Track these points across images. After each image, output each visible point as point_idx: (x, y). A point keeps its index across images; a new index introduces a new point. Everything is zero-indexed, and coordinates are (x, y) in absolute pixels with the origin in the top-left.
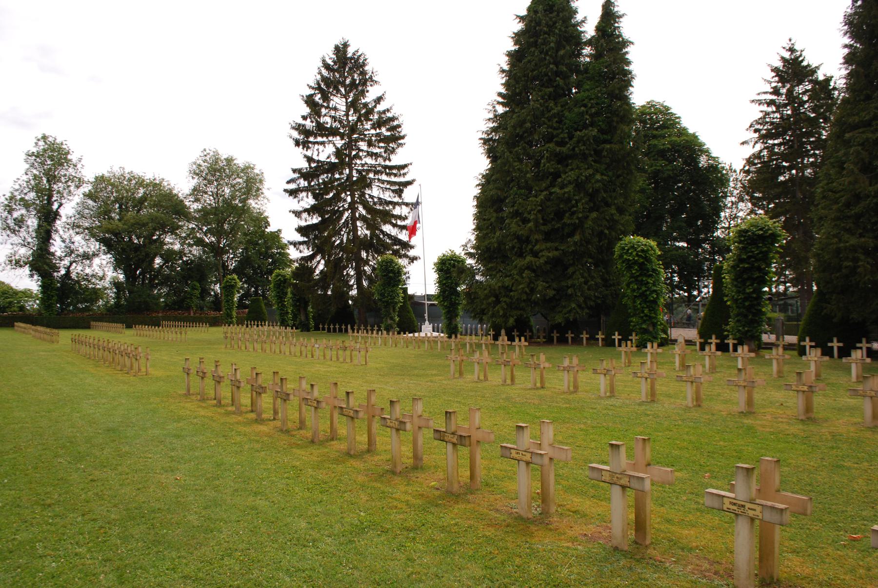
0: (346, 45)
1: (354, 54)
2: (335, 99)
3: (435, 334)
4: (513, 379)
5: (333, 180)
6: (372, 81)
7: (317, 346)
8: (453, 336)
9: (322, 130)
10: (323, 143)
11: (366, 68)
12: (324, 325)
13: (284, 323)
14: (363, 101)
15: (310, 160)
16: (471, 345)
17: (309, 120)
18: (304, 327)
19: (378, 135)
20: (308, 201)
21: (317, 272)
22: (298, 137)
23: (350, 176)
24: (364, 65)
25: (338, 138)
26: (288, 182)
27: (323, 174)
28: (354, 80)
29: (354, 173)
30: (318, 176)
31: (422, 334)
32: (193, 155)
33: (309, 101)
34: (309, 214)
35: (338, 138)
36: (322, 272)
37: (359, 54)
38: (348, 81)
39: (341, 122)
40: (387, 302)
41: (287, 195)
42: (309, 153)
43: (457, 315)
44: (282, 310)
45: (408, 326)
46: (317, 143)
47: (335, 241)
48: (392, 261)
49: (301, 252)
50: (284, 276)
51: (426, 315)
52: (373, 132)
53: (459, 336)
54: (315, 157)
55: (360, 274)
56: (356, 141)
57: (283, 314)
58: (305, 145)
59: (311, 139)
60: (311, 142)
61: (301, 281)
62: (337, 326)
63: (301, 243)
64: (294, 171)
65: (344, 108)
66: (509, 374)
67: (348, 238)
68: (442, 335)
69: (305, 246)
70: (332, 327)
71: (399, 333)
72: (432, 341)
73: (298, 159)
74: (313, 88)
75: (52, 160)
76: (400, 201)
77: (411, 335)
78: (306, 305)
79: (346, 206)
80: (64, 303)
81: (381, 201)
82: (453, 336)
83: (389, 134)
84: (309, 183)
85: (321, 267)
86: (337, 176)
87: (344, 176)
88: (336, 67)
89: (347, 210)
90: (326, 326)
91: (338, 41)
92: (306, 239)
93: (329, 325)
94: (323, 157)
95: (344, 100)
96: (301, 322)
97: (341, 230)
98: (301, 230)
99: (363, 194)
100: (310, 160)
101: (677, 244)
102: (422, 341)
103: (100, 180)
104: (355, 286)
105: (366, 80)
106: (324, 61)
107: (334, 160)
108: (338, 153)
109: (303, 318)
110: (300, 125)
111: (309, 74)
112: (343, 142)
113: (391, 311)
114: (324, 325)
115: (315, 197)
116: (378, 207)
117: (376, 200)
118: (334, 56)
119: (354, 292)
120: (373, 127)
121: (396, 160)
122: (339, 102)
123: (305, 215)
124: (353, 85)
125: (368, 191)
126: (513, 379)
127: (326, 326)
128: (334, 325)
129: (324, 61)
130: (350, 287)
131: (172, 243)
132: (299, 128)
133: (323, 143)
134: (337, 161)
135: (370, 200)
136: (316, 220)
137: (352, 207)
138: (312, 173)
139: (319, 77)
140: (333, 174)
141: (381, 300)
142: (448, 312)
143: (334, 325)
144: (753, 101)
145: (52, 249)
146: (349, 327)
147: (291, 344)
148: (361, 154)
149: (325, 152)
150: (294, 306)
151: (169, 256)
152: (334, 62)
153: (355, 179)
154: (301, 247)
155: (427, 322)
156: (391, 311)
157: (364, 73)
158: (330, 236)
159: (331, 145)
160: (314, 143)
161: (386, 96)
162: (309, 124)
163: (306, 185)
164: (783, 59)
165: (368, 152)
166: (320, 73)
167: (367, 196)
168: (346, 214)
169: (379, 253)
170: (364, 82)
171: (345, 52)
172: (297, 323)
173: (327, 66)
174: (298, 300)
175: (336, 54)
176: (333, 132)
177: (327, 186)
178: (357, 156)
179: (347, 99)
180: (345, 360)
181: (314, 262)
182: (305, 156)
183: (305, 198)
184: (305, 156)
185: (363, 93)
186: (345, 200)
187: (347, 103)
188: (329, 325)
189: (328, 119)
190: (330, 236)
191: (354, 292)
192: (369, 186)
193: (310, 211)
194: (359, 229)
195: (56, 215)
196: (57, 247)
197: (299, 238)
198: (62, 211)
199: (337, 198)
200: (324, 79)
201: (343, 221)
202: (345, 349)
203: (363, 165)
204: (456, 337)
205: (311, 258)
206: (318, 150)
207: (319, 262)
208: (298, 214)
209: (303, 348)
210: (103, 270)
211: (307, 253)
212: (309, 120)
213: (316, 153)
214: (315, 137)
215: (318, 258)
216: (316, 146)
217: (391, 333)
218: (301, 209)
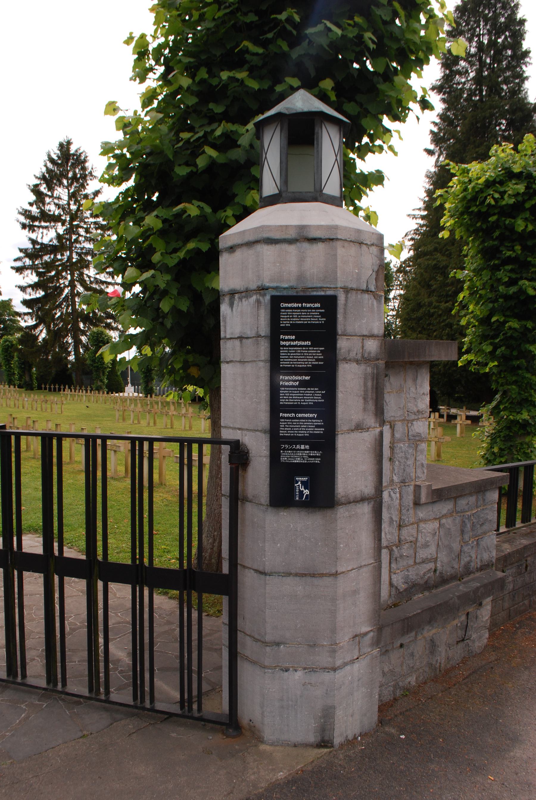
0: (69, 143)
1: (76, 151)
2: (58, 189)
3: (136, 394)
4: (155, 423)
5: (55, 260)
6: (92, 175)
7: (26, 399)
8: (149, 396)
9: (45, 216)
10: (46, 227)
11: (87, 165)
12: (45, 385)
13: (10, 382)
14: (84, 193)
15: (34, 242)
16: (162, 403)
17: (35, 206)
18: (28, 386)
19: (95, 223)
20: (33, 278)
21: (40, 339)
22: (24, 221)
23: (70, 258)
24: (85, 161)
25: (60, 224)
26: (15, 260)
27: (46, 254)
28: (75, 174)
29: (75, 256)
30: (41, 257)
31: (126, 394)
33: (35, 190)
34: (33, 289)
35: (60, 224)
36: (44, 339)
37: (81, 151)
38: (70, 175)
39: (64, 209)
40: (97, 367)
41: (14, 271)
42: (33, 236)
43: (153, 380)
44: (8, 371)
45: (115, 386)
46: (43, 227)
47: (56, 314)
48: (102, 333)
49: (25, 321)
50: (11, 342)
51: (129, 379)
52: (92, 220)
53: (153, 396)
54: (39, 240)
55: (77, 342)
56: (78, 226)
57: (10, 374)
58: (32, 228)
59: (37, 223)
60: (36, 226)
61: (25, 346)
62: (57, 386)
63: (25, 314)
64: (21, 250)
65: (66, 198)
66: (169, 421)
67: (67, 311)
68: (141, 395)
69: (29, 317)
70: (52, 387)
71: (108, 393)
72: (133, 400)
73: (23, 239)
74: (39, 178)
76: (113, 282)
77: (117, 394)
78: (30, 368)
79: (67, 283)
81: (98, 281)
82: (149, 396)
84: (33, 262)
85: (43, 335)
86: (59, 257)
87: (65, 258)
88: (60, 162)
89: (68, 287)
90: (48, 386)
91: (62, 139)
92: (31, 311)
93: (50, 385)
94: (46, 241)
95: (66, 190)
96: (25, 382)
97: (62, 304)
98: (26, 303)
99: (82, 274)
100: (34, 242)
102: (124, 400)
104: (73, 353)
105: (86, 176)
106: (49, 156)
107: (55, 242)
108: (59, 237)
109: (27, 379)
110: (26, 211)
111: (38, 167)
112: (65, 228)
113: (101, 375)
114: (45, 385)
115: (39, 274)
116: (94, 286)
117: (92, 279)
118: (58, 152)
119: (72, 358)
120: (92, 216)
122: (62, 193)
123: (29, 290)
124: (75, 178)
125: (86, 272)
126: (155, 423)
127: (48, 386)
128: (55, 385)
129: (49, 156)
130: (69, 354)
132: (26, 214)
133: (46, 227)
134: (57, 244)
135: (87, 279)
136: (40, 293)
137: (72, 284)
138: (36, 252)
139: (44, 170)
140: (55, 255)
141: (92, 365)
142: (146, 377)
143: (55, 385)
144: (409, 215)
146: (67, 387)
147: (7, 398)
148: (80, 238)
149: (48, 236)
150: (20, 368)
152: (58, 156)
153: (74, 260)
154: (26, 317)
155: (130, 385)
156: (101, 375)
157: (84, 169)
158: (51, 310)
159: (54, 230)
160: (39, 227)
161: (103, 190)
162: (34, 210)
163: (31, 264)
164: (371, 190)
165: (85, 237)
166: (46, 166)
167: (85, 276)
168: (66, 291)
169: (95, 325)
170: (84, 177)
171: (68, 149)
172: (22, 383)
173: (52, 160)
174: (23, 363)
175: (60, 150)
176: (56, 219)
177: (48, 266)
178: (77, 241)
179: (69, 190)
180: (46, 410)
181: (37, 331)
182: (30, 239)
183: (30, 275)
184: (30, 239)
185: (83, 186)
186: (66, 278)
187: (69, 193)
188: (50, 385)
189: (52, 208)
190: (51, 310)
191: (72, 358)
192: (87, 267)
193: (35, 286)
194: (77, 304)
197: (25, 309)
199: (58, 275)
200: (49, 171)
201: (63, 296)
202: (46, 401)
203: (82, 249)
204: (151, 396)
205: (35, 327)
206: (42, 233)
207: (41, 331)
208: (23, 289)
209: (16, 402)
211: (31, 322)
212: (35, 206)
213: (40, 236)
214: (40, 222)
215: (41, 327)
216: (41, 230)
217: (101, 393)
218: (26, 285)
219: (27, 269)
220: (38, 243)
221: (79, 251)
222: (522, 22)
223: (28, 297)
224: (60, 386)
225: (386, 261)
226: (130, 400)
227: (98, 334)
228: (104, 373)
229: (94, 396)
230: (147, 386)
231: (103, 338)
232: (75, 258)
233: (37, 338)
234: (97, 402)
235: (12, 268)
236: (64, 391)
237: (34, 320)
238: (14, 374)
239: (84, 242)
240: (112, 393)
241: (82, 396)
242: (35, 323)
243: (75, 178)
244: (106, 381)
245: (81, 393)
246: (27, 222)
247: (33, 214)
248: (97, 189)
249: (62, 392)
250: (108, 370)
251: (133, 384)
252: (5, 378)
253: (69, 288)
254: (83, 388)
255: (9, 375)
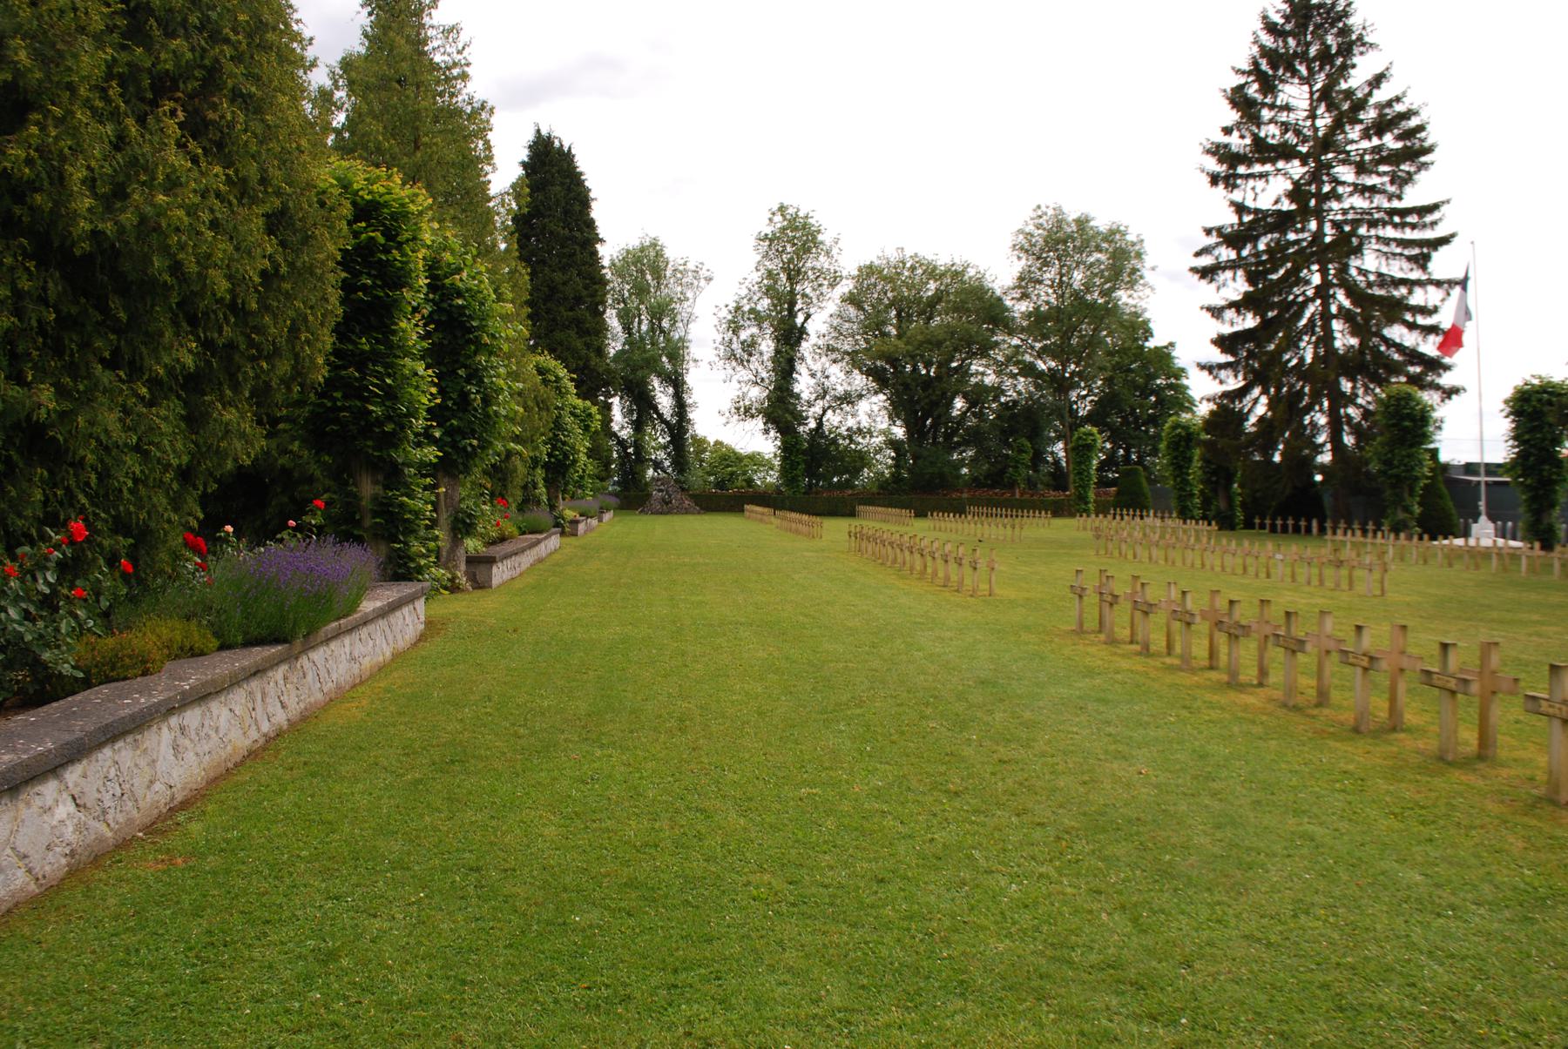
3: (1500, 542)
9: (1263, 151)
10: (1262, 176)
12: (1263, 518)
13: (1185, 514)
15: (1240, 209)
17: (1236, 134)
21: (1253, 419)
23: (1319, 234)
26: (1198, 254)
29: (1328, 229)
33: (1238, 99)
34: (1238, 312)
36: (1262, 419)
40: (1397, 476)
42: (1237, 196)
44: (1182, 489)
52: (1365, 144)
54: (1250, 203)
58: (1230, 181)
59: (1241, 170)
62: (1290, 522)
64: (1208, 232)
70: (1279, 522)
76: (1424, 277)
77: (1446, 542)
78: (1230, 479)
79: (1310, 293)
85: (1261, 409)
90: (1268, 522)
92: (1231, 359)
93: (1273, 519)
94: (1265, 203)
100: (1240, 209)
107: (1286, 205)
109: (1222, 505)
110: (1218, 146)
114: (1263, 518)
123: (1230, 314)
124: (1325, 56)
127: (1268, 522)
128: (1285, 519)
130: (1318, 449)
133: (1262, 176)
136: (1250, 321)
142: (1533, 499)
143: (1285, 519)
148: (1340, 190)
149: (1270, 191)
153: (1328, 239)
154: (1223, 374)
156: (1406, 495)
157: (1345, 32)
161: (1392, 71)
162: (1237, 142)
170: (1347, 50)
173: (1271, 28)
174: (1214, 473)
182: (1233, 203)
183: (1230, 282)
184: (1233, 203)
185: (1344, 70)
186: (1307, 282)
188: (1273, 519)
189: (1273, 130)
191: (1325, 458)
199: (1293, 278)
203: (1345, 212)
205: (1241, 393)
207: (1256, 401)
208: (1216, 312)
213: (1250, 195)
215: (1256, 391)
216: (1251, 183)
218: (1223, 303)
219: (1224, 269)
220: (1249, 211)
221: (1339, 217)
222: (860, 269)
223: (1227, 330)
224: (1297, 520)
225: (1151, 344)
226: (1499, 555)
227: (1398, 400)
228: (1412, 492)
229: (1389, 545)
230: (1538, 521)
231: (1413, 408)
232: (1329, 235)
233: (1243, 417)
234: (1425, 562)
235: (1194, 270)
236: (1334, 533)
237: (1240, 377)
238: (1192, 495)
239: (1351, 194)
240: (1433, 538)
241: (1344, 543)
242: (1242, 384)
243: (1325, 56)
244: (1417, 510)
245: (1379, 540)
246: (1221, 169)
247: (1234, 149)
248: (1378, 71)
249: (1329, 536)
250: (1422, 483)
251: (1492, 518)
252: (1173, 503)
253: (1318, 302)
254: (1356, 526)
255: (1181, 499)
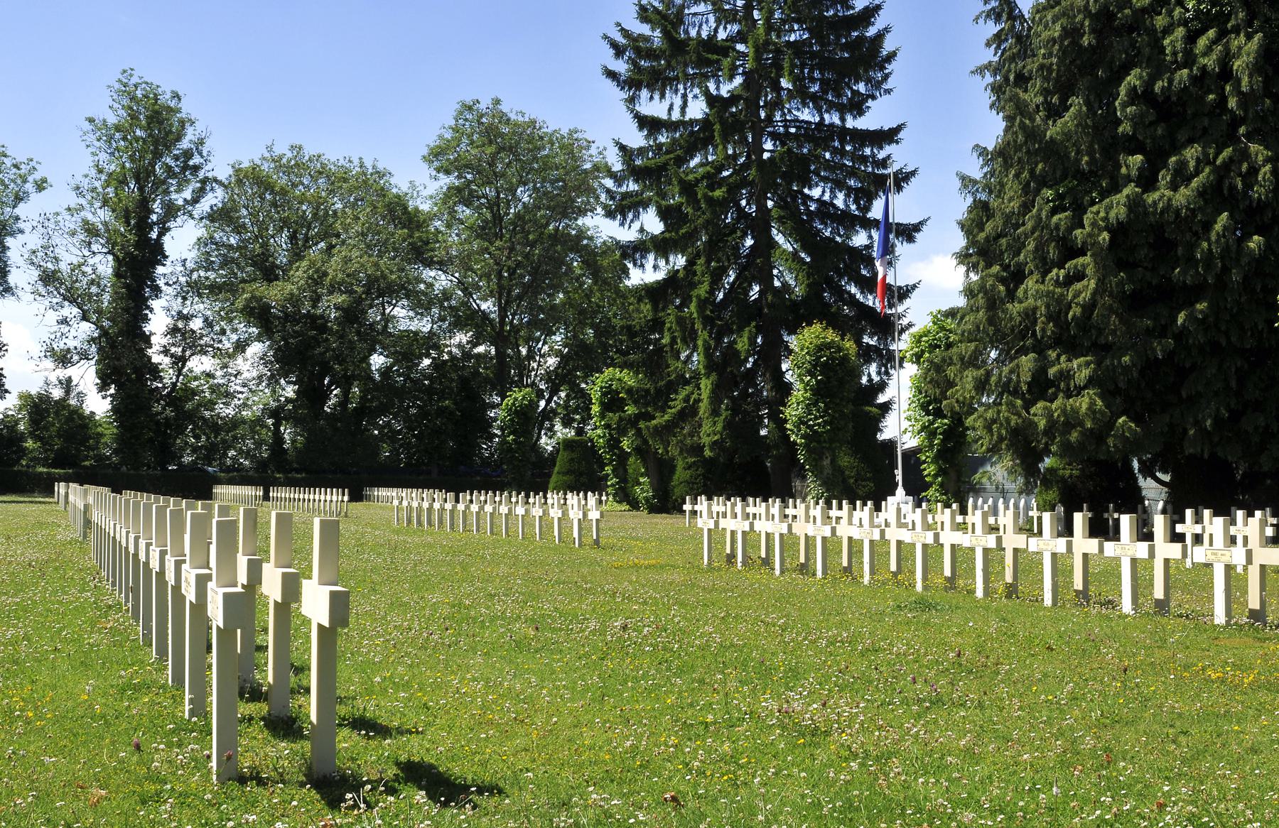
32: (437, 123)
51: (899, 474)
75: (151, 142)
80: (156, 444)
83: (738, 80)
100: (650, 125)
101: (933, 279)
103: (248, 177)
121: (874, 118)
131: (403, 317)
145: (147, 329)
151: (408, 348)
155: (900, 491)
195: (156, 253)
196: (158, 323)
198: (169, 243)
210: (241, 375)
